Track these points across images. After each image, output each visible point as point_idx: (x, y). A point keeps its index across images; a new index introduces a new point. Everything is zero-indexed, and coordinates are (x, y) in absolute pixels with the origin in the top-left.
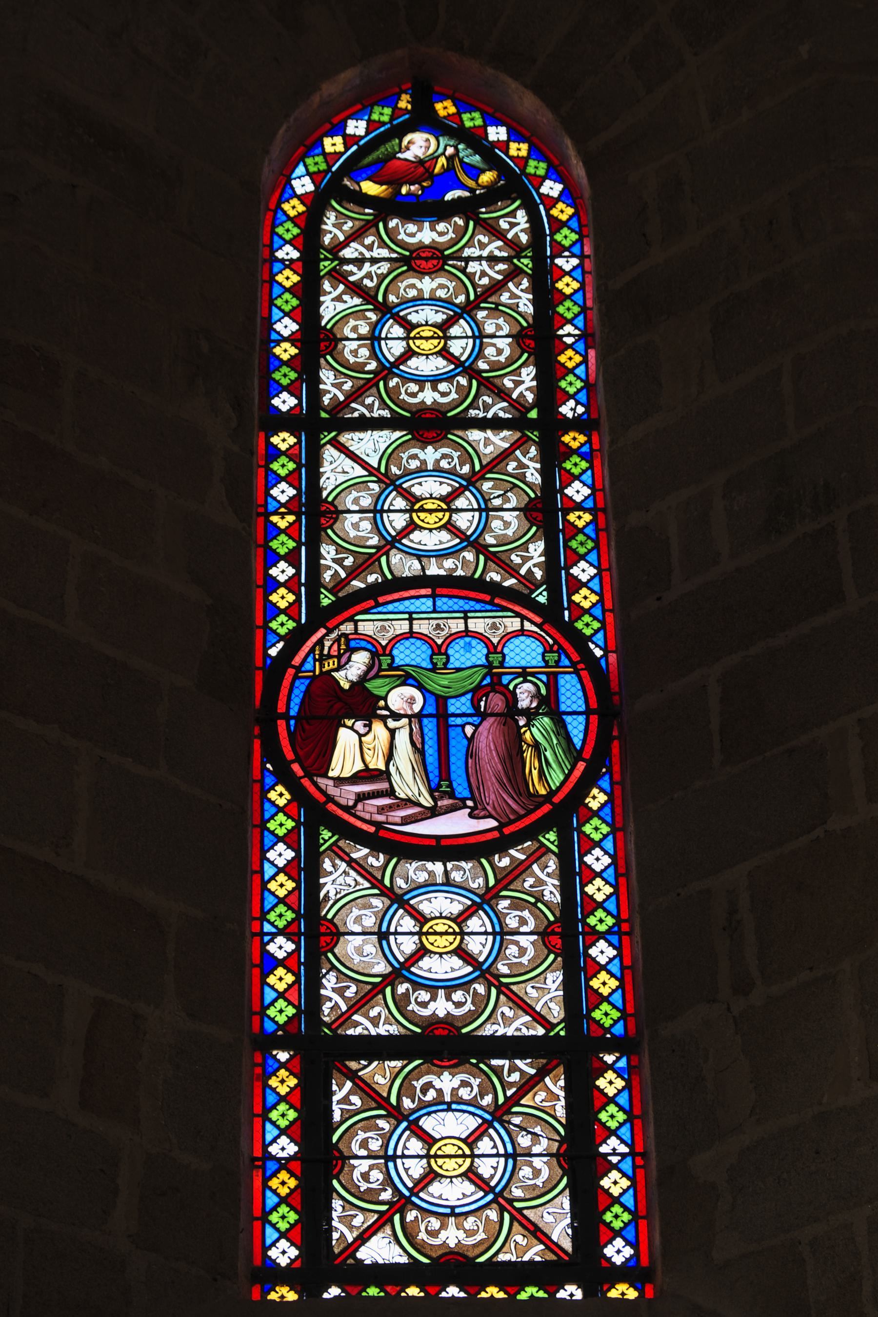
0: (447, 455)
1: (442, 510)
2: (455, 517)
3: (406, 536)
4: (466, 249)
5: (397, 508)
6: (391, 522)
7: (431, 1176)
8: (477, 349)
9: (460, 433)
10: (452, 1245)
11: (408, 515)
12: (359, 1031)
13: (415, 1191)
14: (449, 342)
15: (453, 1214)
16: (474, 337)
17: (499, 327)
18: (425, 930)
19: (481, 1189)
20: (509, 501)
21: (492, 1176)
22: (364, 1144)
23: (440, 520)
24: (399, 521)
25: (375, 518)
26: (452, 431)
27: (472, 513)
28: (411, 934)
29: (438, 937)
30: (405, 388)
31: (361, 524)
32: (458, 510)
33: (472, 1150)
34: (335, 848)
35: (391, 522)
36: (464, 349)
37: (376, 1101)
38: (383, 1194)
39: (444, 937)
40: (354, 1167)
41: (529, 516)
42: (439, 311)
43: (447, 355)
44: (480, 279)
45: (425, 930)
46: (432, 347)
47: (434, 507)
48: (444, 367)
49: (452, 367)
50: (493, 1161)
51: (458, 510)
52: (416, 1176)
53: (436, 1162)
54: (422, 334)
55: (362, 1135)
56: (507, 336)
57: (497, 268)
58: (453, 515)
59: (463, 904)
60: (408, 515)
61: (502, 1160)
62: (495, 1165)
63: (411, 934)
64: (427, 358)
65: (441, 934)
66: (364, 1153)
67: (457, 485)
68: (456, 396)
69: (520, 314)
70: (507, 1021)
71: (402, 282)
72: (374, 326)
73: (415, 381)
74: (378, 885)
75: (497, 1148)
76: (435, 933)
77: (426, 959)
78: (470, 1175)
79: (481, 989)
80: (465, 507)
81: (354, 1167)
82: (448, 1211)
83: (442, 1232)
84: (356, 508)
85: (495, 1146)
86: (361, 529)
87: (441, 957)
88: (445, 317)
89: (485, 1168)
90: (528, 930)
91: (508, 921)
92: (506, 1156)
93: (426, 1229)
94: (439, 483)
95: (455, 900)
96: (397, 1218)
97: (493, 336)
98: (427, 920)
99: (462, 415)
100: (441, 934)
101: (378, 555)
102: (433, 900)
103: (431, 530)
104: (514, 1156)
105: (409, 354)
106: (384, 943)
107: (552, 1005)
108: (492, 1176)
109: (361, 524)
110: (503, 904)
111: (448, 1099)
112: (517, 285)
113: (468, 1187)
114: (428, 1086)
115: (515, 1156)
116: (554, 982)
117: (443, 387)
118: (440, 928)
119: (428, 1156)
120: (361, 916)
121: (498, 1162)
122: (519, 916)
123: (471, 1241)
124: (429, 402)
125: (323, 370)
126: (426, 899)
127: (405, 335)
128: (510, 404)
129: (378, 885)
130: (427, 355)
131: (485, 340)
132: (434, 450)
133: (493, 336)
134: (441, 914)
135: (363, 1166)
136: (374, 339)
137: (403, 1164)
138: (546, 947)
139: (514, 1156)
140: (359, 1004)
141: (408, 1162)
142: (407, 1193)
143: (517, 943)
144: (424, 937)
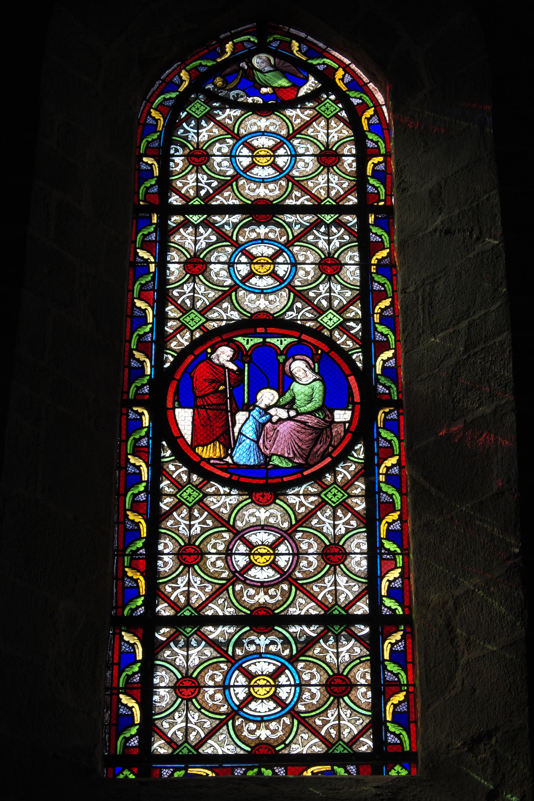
0: (274, 123)
1: (271, 686)
2: (277, 159)
3: (246, 706)
4: (287, 200)
5: (239, 684)
6: (236, 694)
7: (250, 698)
8: (297, 695)
9: (280, 216)
10: (263, 739)
11: (247, 689)
12: (218, 202)
13: (241, 707)
14: (278, 689)
15: (263, 182)
16: (291, 263)
17: (307, 149)
18: (255, 154)
19: (278, 171)
20: (308, 259)
21: (287, 698)
22: (214, 546)
23: (268, 161)
24: (246, 162)
25: (226, 558)
26: (277, 216)
27: (288, 556)
28: (248, 156)
29: (260, 688)
30: (246, 591)
31: (217, 562)
32: (279, 263)
33: (275, 682)
34: (202, 327)
35: (236, 694)
36: (286, 163)
37: (220, 522)
38: (222, 708)
39: (264, 688)
40: (208, 559)
41: (321, 268)
42: (271, 534)
43: (275, 166)
44: (299, 509)
45: (252, 683)
46: (265, 561)
47: (265, 551)
48: (273, 174)
49: (278, 173)
50: (287, 689)
51: (279, 263)
52: (241, 698)
53: (254, 690)
54: (259, 550)
55: (213, 541)
56: (312, 264)
57: (306, 113)
58: (277, 557)
59: (275, 249)
60: (247, 689)
61: (293, 688)
62: (289, 691)
63: (248, 156)
64: (263, 168)
65: (262, 686)
66: (213, 551)
67: (278, 249)
68: (280, 598)
69: (323, 534)
70: (297, 198)
71: (245, 639)
72: (232, 148)
73: (254, 722)
74: (231, 133)
75: (289, 550)
76: (260, 156)
77: (253, 570)
78: (273, 565)
79: (285, 587)
80: (284, 552)
81: (208, 559)
82: (261, 180)
83: (256, 596)
84: (220, 154)
85: (289, 680)
86: (215, 700)
87: (263, 168)
88: (274, 143)
89: (283, 693)
90: (310, 262)
91: (302, 545)
92: (296, 685)
93: (247, 729)
94: (267, 664)
95: (271, 534)
96: (230, 723)
97: (303, 155)
98: (254, 547)
99: (285, 612)
100: (262, 686)
101: (230, 291)
102: (257, 664)
103: (263, 167)
104: (300, 685)
105: (253, 165)
106: (231, 268)
107: (322, 191)
108: (287, 698)
109: (217, 562)
110: (298, 535)
111: (263, 650)
112: (318, 124)
113: (272, 705)
114: (252, 515)
115: (301, 685)
116: (323, 179)
117: (271, 186)
118: (262, 153)
119: (248, 686)
120: (221, 148)
121: (291, 690)
122: (310, 673)
123: (274, 737)
124: (263, 738)
125: (191, 712)
126: (253, 663)
127: (247, 683)
128: (313, 308)
129: (231, 133)
130: (262, 567)
131: (298, 266)
132: (265, 638)
133: (303, 155)
134: (262, 672)
135: (218, 160)
136: (232, 156)
137: (234, 690)
138: (319, 162)
139: (300, 685)
140: (212, 597)
141: (237, 690)
142: (236, 708)
143: (304, 269)
144: (251, 688)
